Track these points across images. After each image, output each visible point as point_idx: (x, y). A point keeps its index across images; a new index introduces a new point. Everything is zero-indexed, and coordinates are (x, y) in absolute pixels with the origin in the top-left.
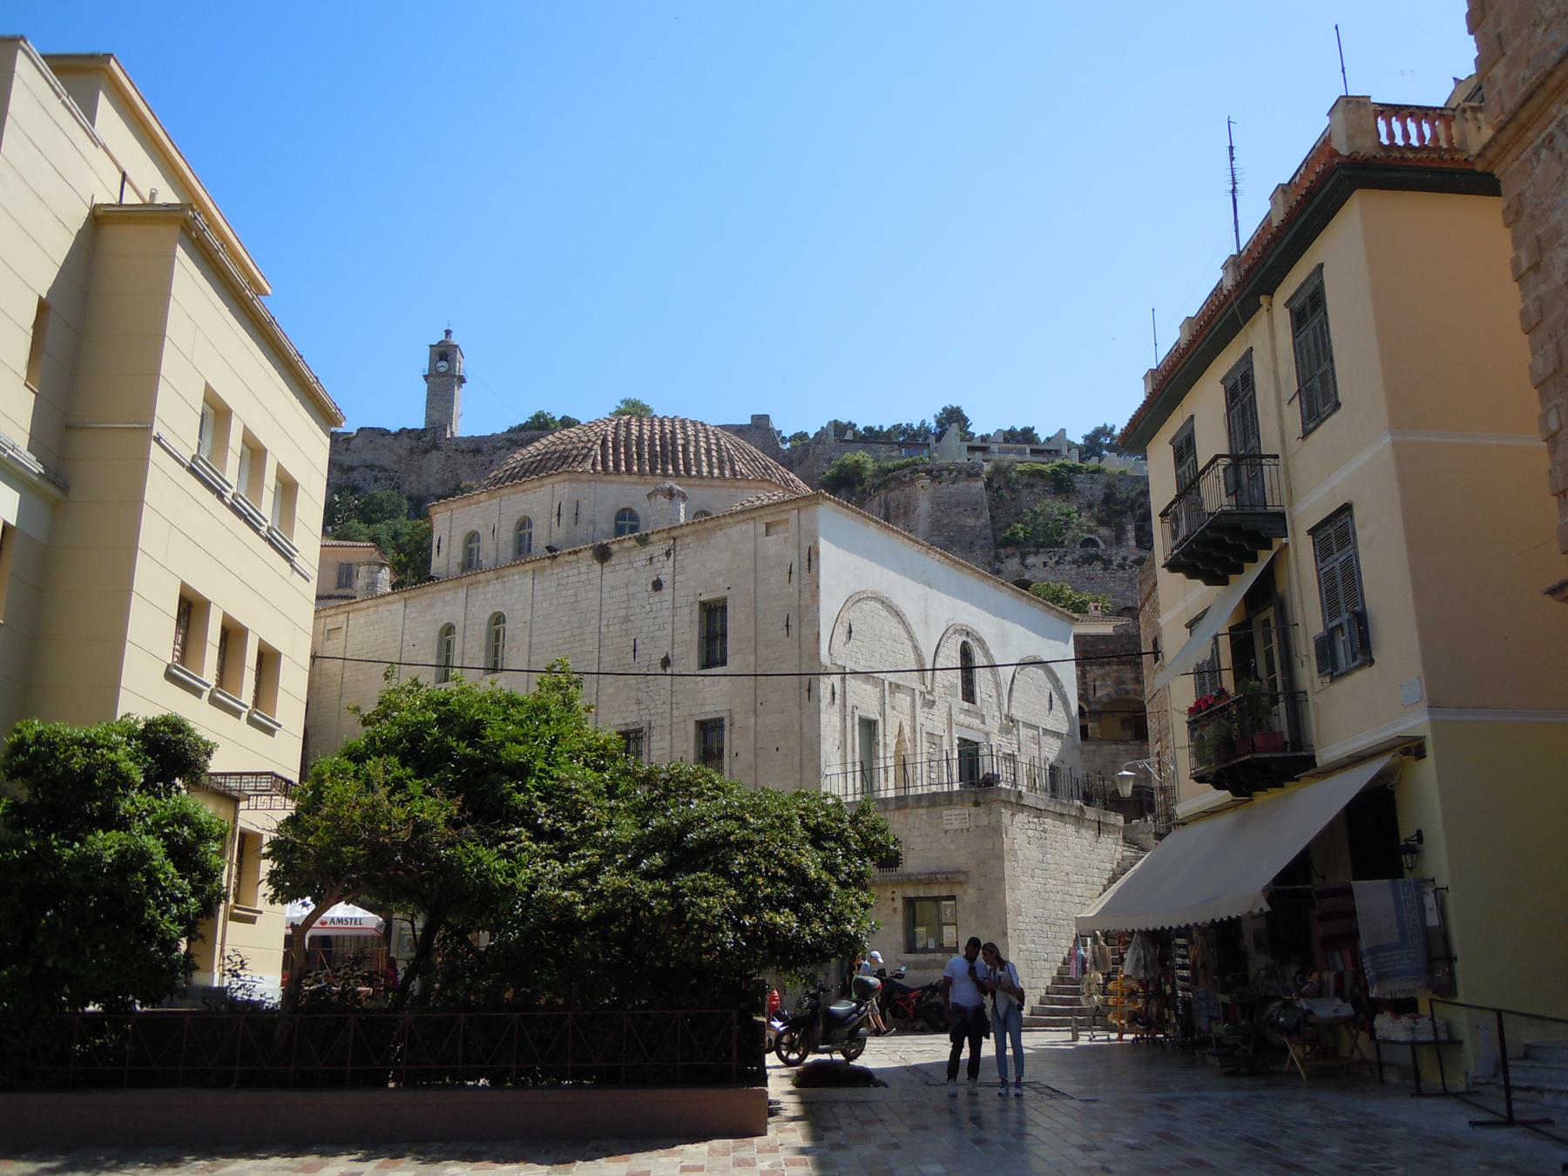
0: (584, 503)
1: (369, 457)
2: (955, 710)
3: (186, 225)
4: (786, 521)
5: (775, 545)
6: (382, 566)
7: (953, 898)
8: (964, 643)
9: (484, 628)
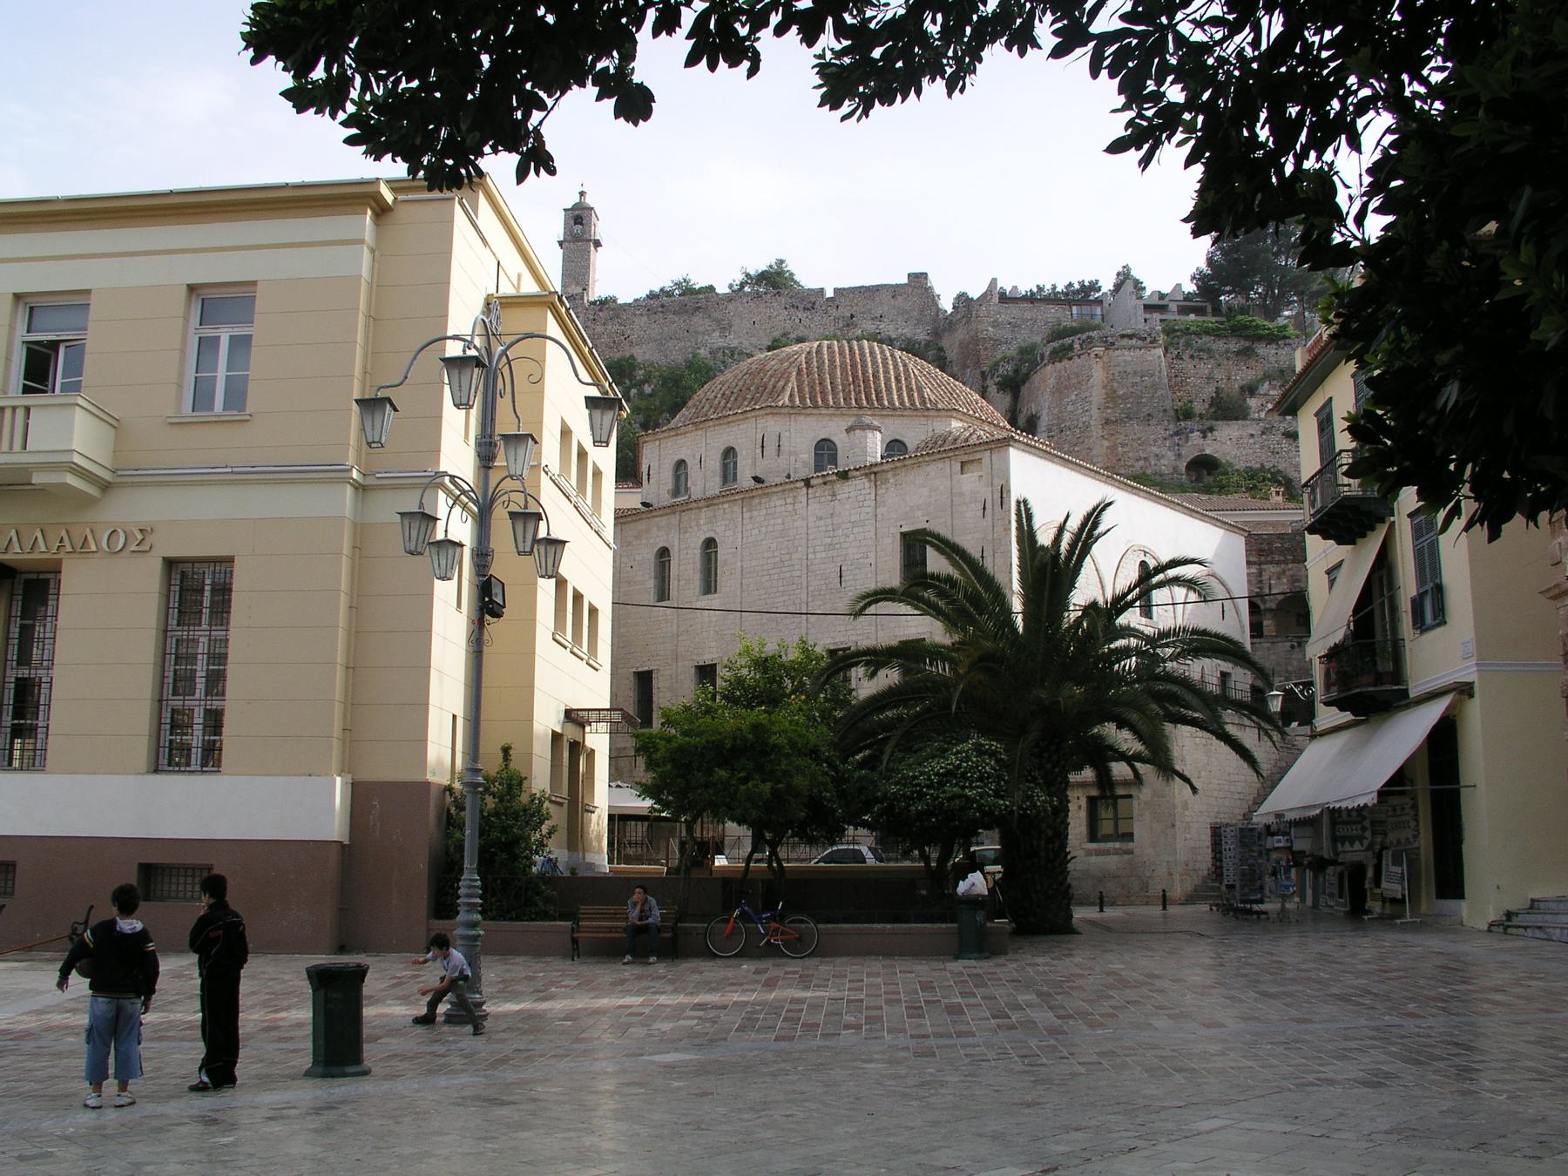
5: (970, 482)
7: (1130, 796)
9: (698, 552)
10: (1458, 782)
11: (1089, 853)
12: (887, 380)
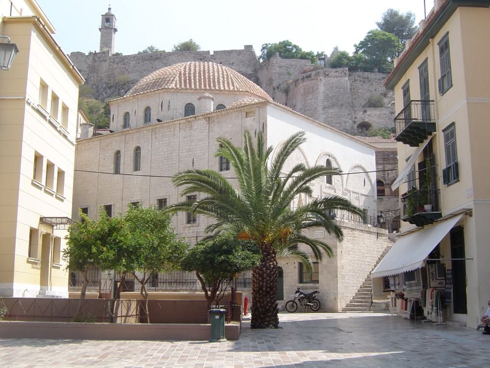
2: (323, 187)
3: (37, 24)
4: (254, 112)
6: (92, 125)
9: (132, 152)
10: (464, 258)
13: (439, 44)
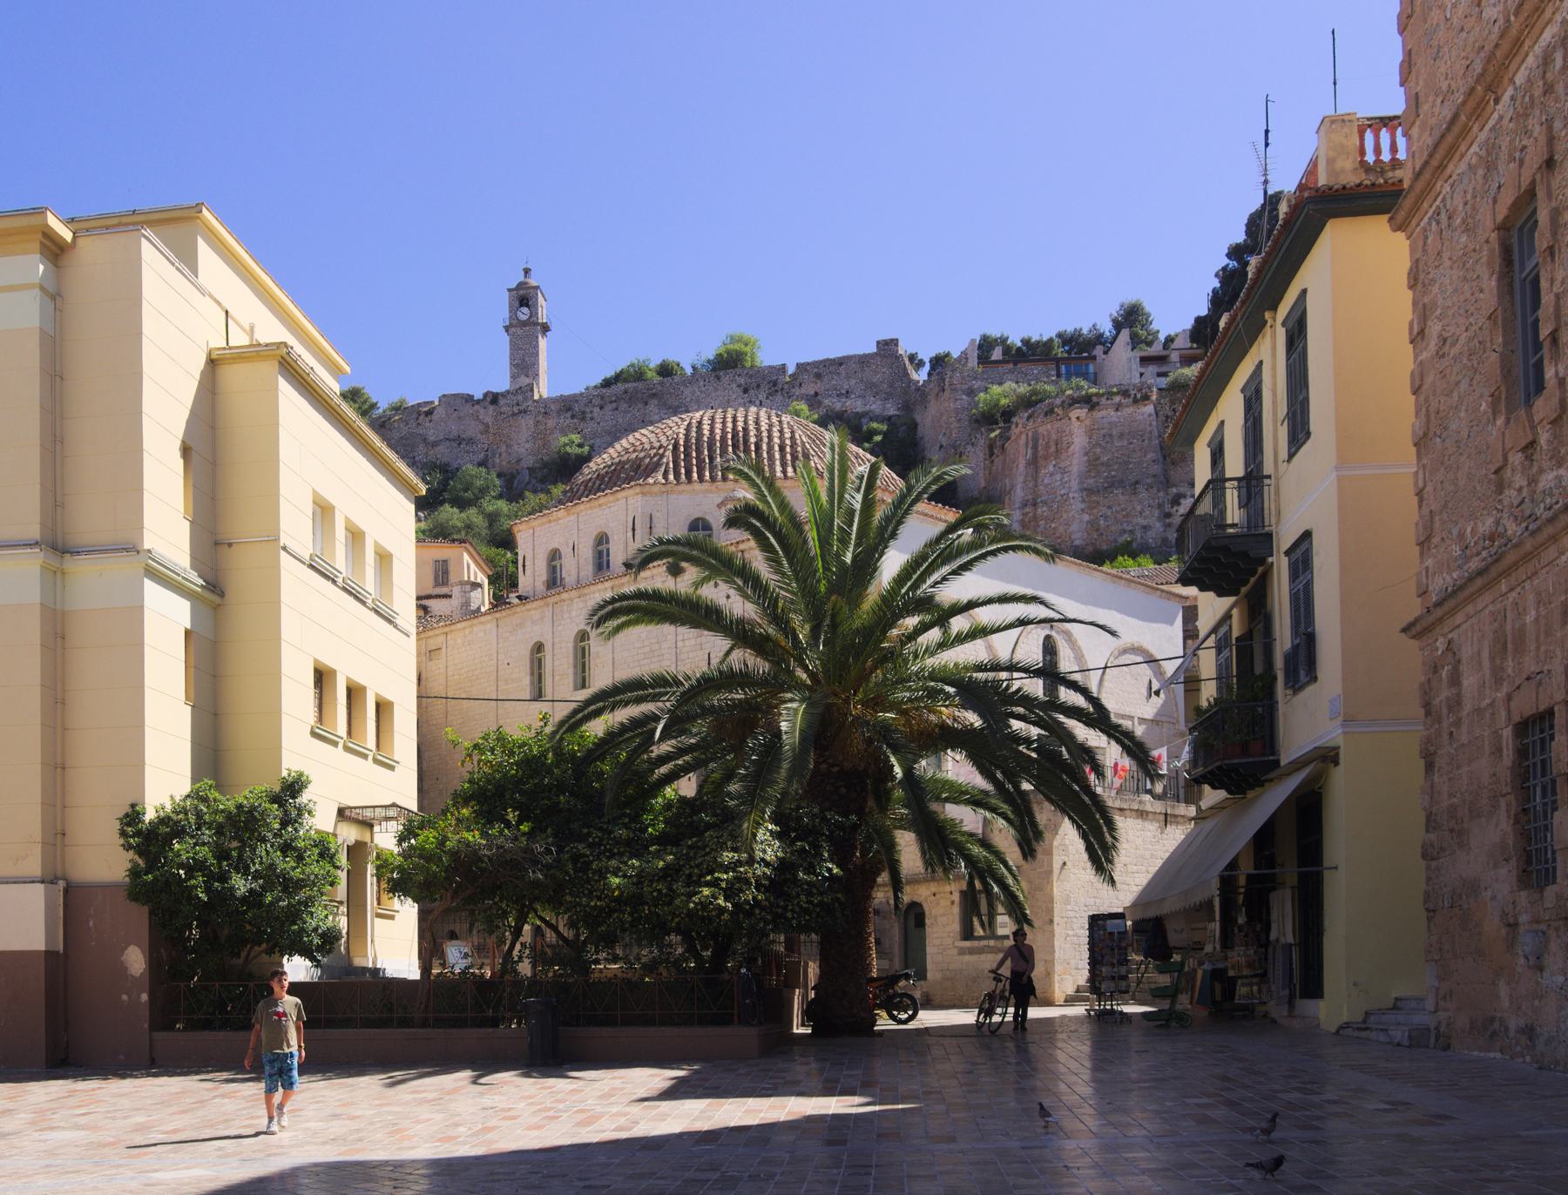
0: (656, 516)
1: (454, 429)
8: (1048, 638)
9: (571, 645)
10: (1321, 864)
11: (962, 952)
12: (770, 448)
13: (1284, 324)
